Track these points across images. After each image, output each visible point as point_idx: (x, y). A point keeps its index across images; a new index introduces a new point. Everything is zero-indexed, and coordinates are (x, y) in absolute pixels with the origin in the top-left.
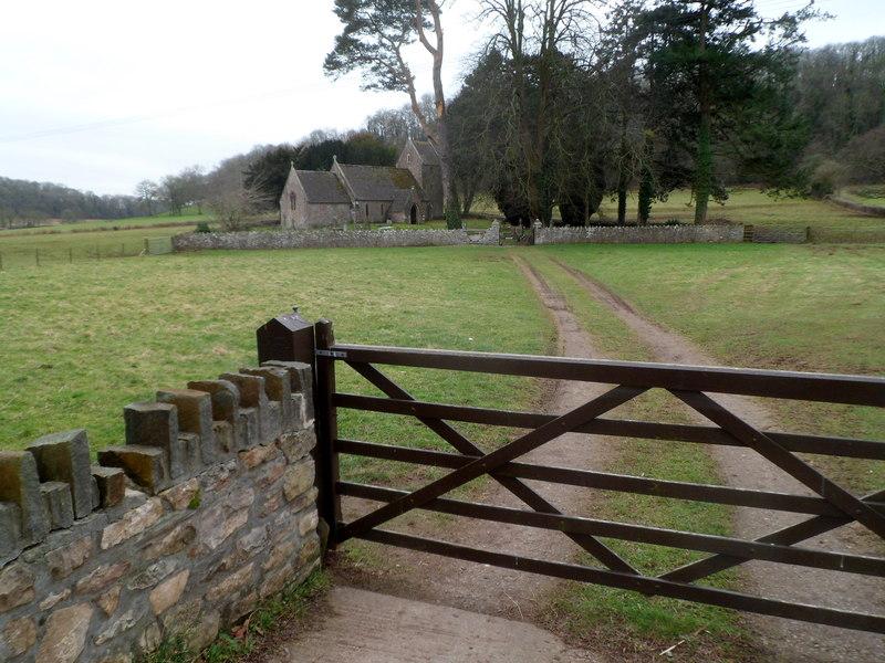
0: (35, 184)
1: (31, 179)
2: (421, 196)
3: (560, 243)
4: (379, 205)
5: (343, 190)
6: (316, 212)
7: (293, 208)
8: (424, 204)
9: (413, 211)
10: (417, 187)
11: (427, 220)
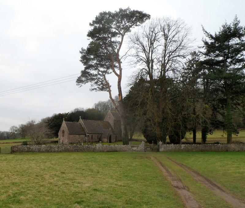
5: (83, 129)
7: (63, 136)
8: (115, 135)
10: (112, 129)
11: (116, 141)
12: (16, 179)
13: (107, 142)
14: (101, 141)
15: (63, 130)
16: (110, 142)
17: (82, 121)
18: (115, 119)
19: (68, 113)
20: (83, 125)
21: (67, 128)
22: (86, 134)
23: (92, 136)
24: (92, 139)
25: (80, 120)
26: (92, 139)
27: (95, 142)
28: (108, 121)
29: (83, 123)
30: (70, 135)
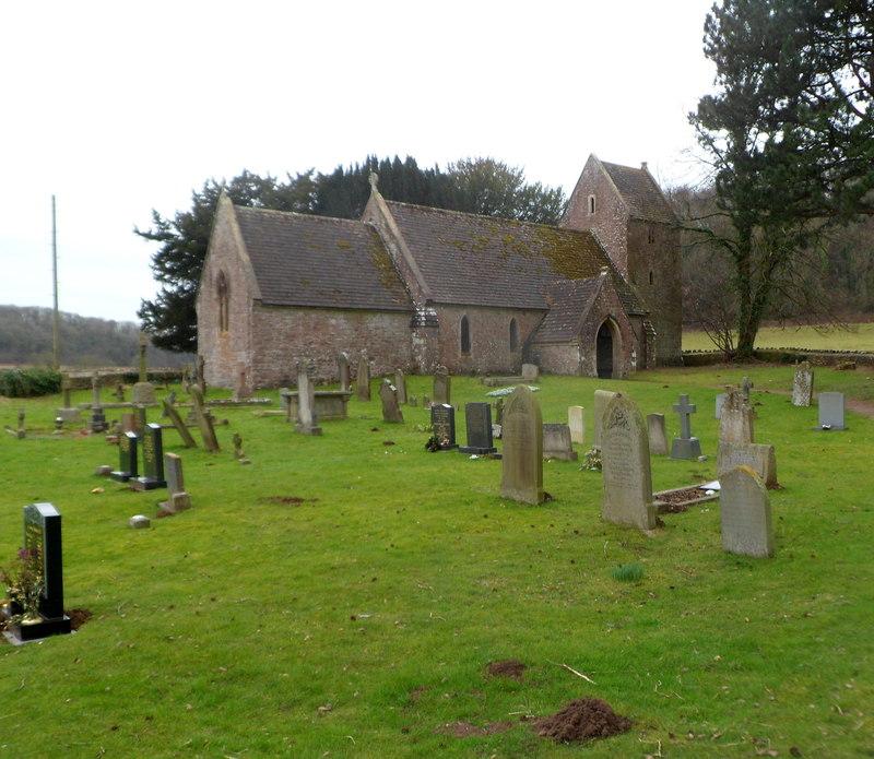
0: (112, 324)
1: (107, 317)
2: (625, 299)
3: (122, 490)
4: (507, 319)
5: (394, 275)
6: (291, 337)
7: (223, 323)
8: (637, 325)
9: (604, 340)
10: (613, 271)
11: (642, 367)
12: (59, 688)
13: (583, 371)
14: (536, 362)
15: (222, 276)
16: (605, 371)
17: (384, 209)
18: (638, 214)
19: (311, 173)
20: (393, 237)
21: (245, 257)
22: (412, 312)
23: (465, 323)
24: (466, 346)
25: (371, 205)
26: (466, 346)
27: (489, 373)
28: (582, 228)
29: (393, 225)
30: (264, 315)
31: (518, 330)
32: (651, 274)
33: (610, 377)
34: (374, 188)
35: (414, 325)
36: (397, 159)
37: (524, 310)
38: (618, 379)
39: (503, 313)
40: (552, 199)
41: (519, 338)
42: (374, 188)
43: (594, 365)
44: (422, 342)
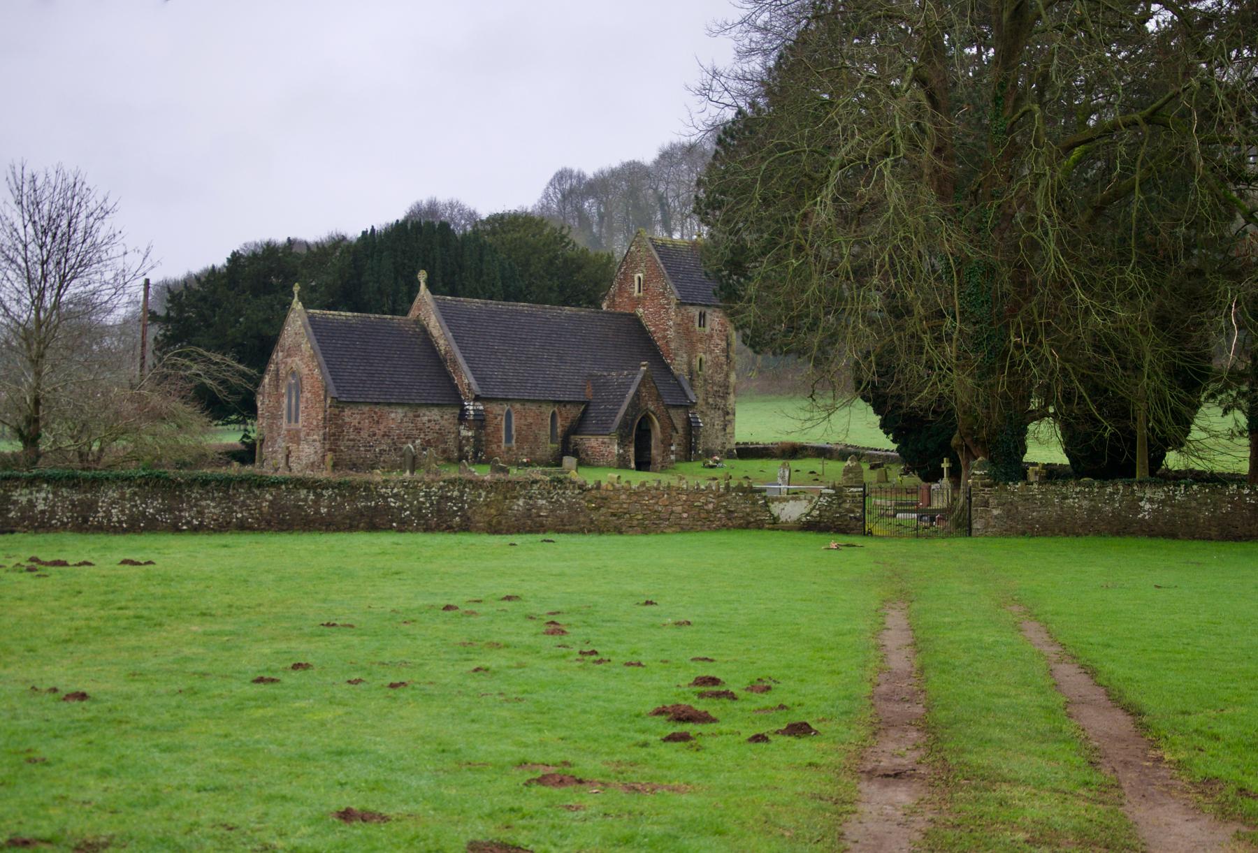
4: (548, 410)
16: (643, 464)
18: (765, 78)
31: (559, 422)
32: (701, 360)
33: (647, 470)
34: (423, 286)
35: (462, 417)
36: (373, 229)
37: (564, 403)
38: (656, 471)
39: (544, 406)
40: (881, 420)
41: (559, 430)
42: (423, 286)
43: (632, 458)
44: (470, 434)
